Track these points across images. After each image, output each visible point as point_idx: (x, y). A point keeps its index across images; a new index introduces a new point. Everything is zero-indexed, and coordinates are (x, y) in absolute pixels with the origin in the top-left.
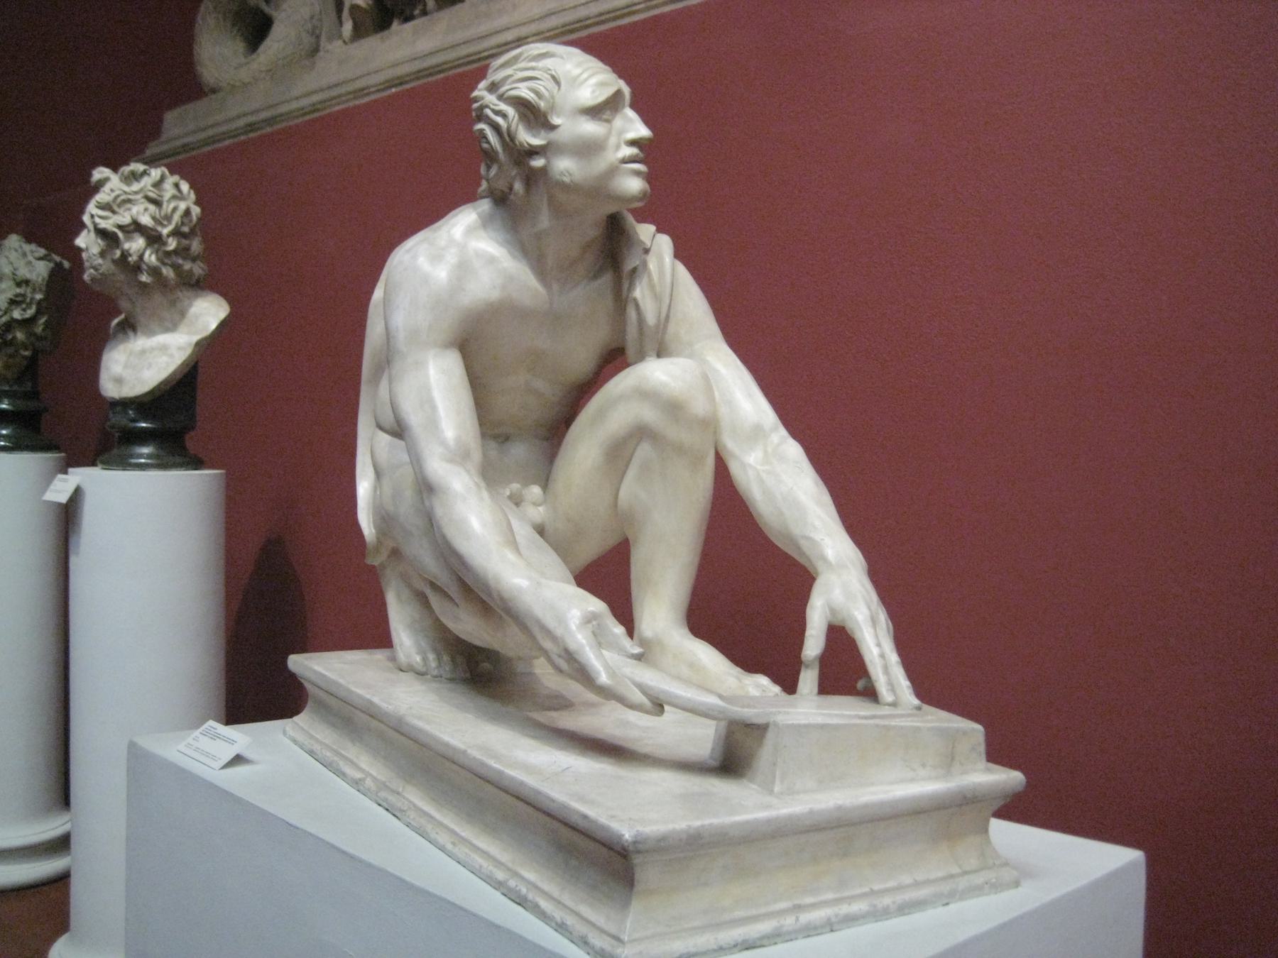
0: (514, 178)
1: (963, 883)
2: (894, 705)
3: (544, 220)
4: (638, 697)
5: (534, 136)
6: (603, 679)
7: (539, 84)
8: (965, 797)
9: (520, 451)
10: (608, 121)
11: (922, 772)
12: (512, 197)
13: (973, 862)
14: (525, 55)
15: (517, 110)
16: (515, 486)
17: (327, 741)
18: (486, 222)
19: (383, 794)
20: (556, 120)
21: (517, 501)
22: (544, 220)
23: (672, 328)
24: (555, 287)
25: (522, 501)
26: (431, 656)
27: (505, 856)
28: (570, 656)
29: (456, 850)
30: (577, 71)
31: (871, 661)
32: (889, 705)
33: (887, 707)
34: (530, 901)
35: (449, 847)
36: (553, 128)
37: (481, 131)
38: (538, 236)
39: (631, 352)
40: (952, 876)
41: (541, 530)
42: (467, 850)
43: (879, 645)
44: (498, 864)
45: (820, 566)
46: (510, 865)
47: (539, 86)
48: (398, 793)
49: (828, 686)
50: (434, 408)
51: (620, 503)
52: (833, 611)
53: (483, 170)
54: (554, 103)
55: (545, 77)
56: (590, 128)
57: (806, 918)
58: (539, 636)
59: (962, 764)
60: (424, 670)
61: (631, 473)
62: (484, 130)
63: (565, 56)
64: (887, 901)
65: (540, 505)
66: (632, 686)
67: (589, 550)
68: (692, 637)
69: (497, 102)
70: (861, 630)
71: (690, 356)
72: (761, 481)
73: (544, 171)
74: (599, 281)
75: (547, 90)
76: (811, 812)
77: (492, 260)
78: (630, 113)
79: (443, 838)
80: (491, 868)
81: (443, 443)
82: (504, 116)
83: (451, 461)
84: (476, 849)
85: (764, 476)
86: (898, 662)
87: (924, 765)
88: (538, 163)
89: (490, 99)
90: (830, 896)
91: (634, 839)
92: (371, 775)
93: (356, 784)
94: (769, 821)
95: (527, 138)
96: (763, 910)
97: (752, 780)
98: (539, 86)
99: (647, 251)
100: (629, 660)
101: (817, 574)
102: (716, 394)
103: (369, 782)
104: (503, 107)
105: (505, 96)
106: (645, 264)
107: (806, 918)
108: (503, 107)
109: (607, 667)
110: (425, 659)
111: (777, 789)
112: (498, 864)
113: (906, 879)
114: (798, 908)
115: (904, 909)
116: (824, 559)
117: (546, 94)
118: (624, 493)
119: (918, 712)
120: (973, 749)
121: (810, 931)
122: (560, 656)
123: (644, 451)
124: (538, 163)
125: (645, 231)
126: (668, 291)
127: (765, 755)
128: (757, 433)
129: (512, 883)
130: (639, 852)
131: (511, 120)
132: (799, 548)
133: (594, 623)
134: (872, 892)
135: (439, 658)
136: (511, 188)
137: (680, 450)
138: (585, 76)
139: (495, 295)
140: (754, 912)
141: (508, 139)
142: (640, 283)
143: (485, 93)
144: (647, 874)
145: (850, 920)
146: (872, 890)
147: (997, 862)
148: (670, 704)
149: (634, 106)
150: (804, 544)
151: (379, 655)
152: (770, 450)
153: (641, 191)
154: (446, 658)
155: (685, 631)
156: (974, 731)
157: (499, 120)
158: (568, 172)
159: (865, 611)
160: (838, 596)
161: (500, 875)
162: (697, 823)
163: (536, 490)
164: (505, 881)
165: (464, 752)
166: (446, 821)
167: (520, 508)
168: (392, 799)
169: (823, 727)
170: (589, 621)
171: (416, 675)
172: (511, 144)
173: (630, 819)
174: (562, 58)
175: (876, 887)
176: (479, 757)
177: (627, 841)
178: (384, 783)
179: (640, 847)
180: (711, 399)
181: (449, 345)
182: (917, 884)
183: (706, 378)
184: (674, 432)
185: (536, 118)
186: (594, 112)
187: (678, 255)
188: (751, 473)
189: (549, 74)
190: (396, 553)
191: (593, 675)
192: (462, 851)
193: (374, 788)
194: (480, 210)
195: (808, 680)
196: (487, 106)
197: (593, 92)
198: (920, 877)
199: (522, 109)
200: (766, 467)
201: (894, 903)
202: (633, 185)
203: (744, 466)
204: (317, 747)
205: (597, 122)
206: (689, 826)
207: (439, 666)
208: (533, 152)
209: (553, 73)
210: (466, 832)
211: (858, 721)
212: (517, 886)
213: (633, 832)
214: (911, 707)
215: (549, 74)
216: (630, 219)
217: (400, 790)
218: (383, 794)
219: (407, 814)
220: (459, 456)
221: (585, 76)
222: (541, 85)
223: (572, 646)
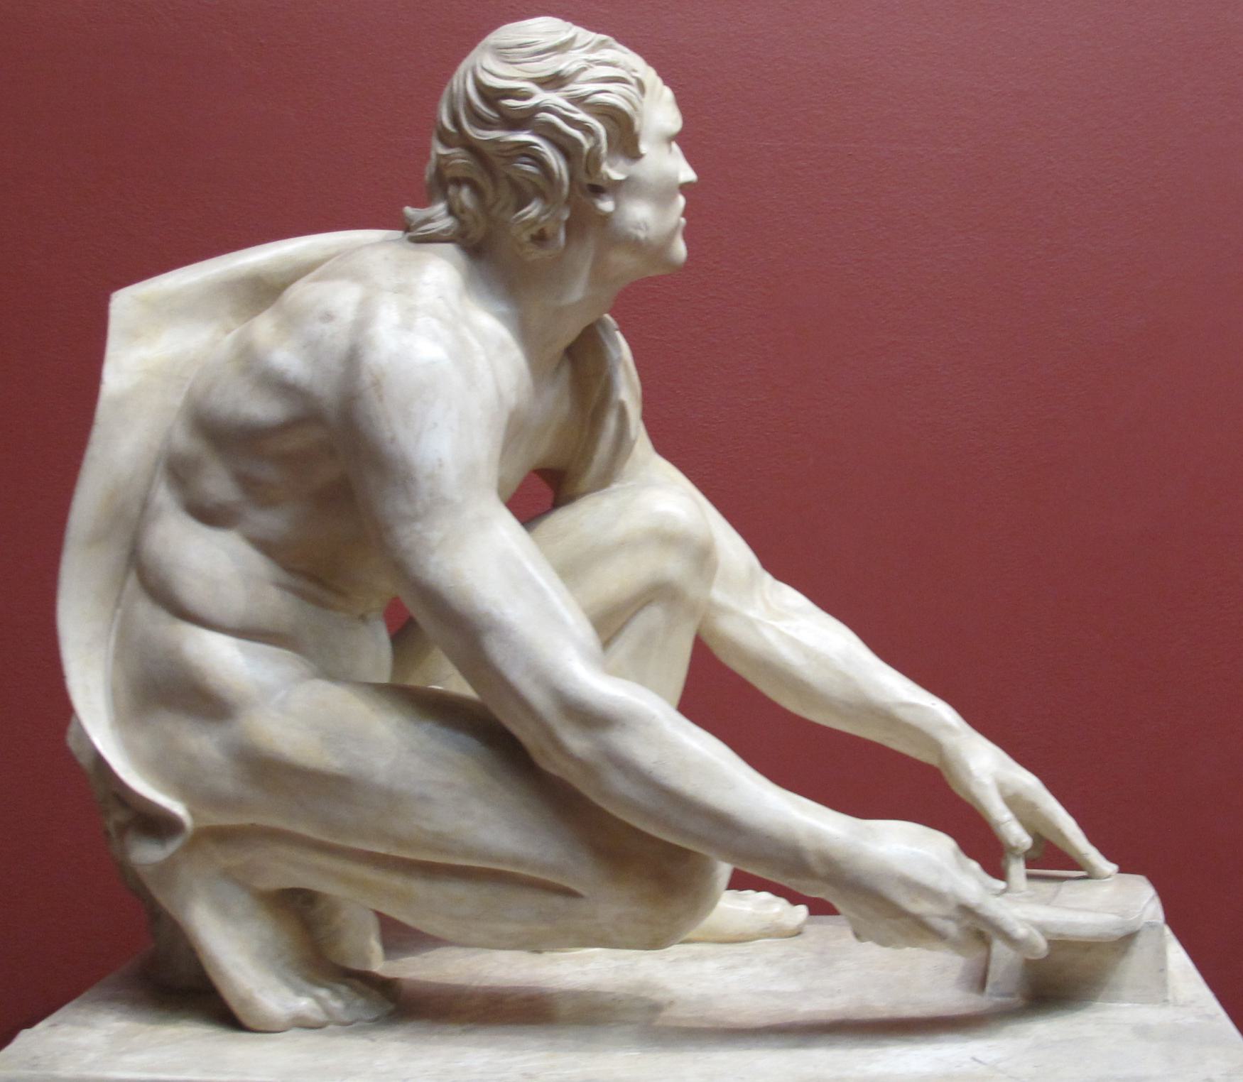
26: (323, 993)
72: (795, 643)
82: (588, 130)
88: (607, 205)
110: (318, 999)
124: (607, 205)
135: (337, 994)
158: (645, 224)
195: (1017, 870)
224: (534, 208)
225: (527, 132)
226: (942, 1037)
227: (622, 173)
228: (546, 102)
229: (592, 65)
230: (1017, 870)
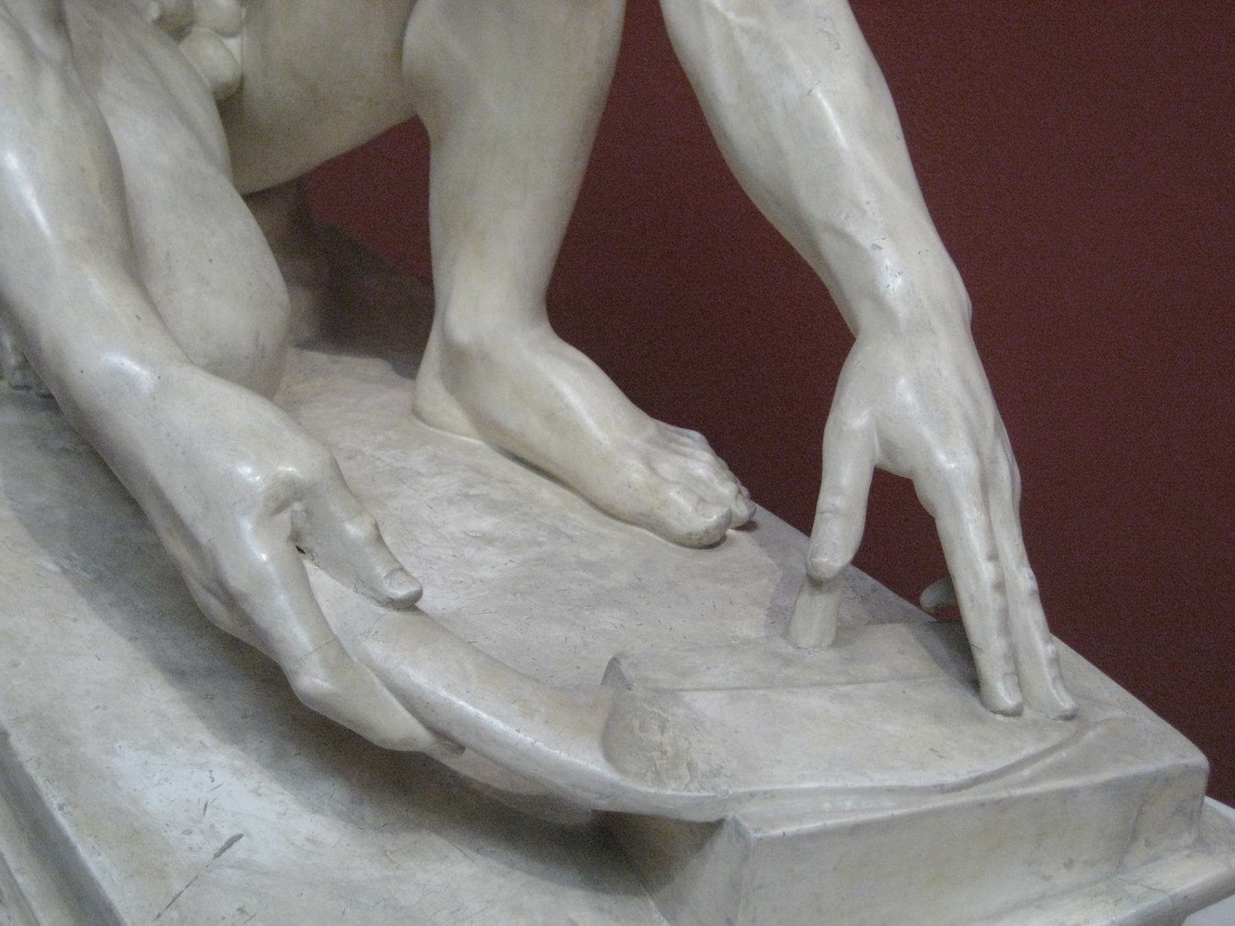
2: (1016, 713)
32: (1005, 713)
33: (999, 717)
43: (994, 557)
45: (864, 318)
51: (407, 58)
52: (888, 446)
59: (1148, 844)
65: (232, 35)
66: (386, 693)
70: (956, 511)
72: (737, 59)
85: (743, 42)
86: (1033, 592)
87: (1069, 865)
116: (879, 302)
118: (412, 39)
119: (1072, 726)
132: (813, 245)
133: (297, 506)
150: (830, 246)
155: (544, 330)
167: (183, 47)
169: (855, 830)
170: (281, 508)
176: (31, 770)
188: (713, 31)
200: (750, 21)
211: (939, 802)
223: (237, 580)
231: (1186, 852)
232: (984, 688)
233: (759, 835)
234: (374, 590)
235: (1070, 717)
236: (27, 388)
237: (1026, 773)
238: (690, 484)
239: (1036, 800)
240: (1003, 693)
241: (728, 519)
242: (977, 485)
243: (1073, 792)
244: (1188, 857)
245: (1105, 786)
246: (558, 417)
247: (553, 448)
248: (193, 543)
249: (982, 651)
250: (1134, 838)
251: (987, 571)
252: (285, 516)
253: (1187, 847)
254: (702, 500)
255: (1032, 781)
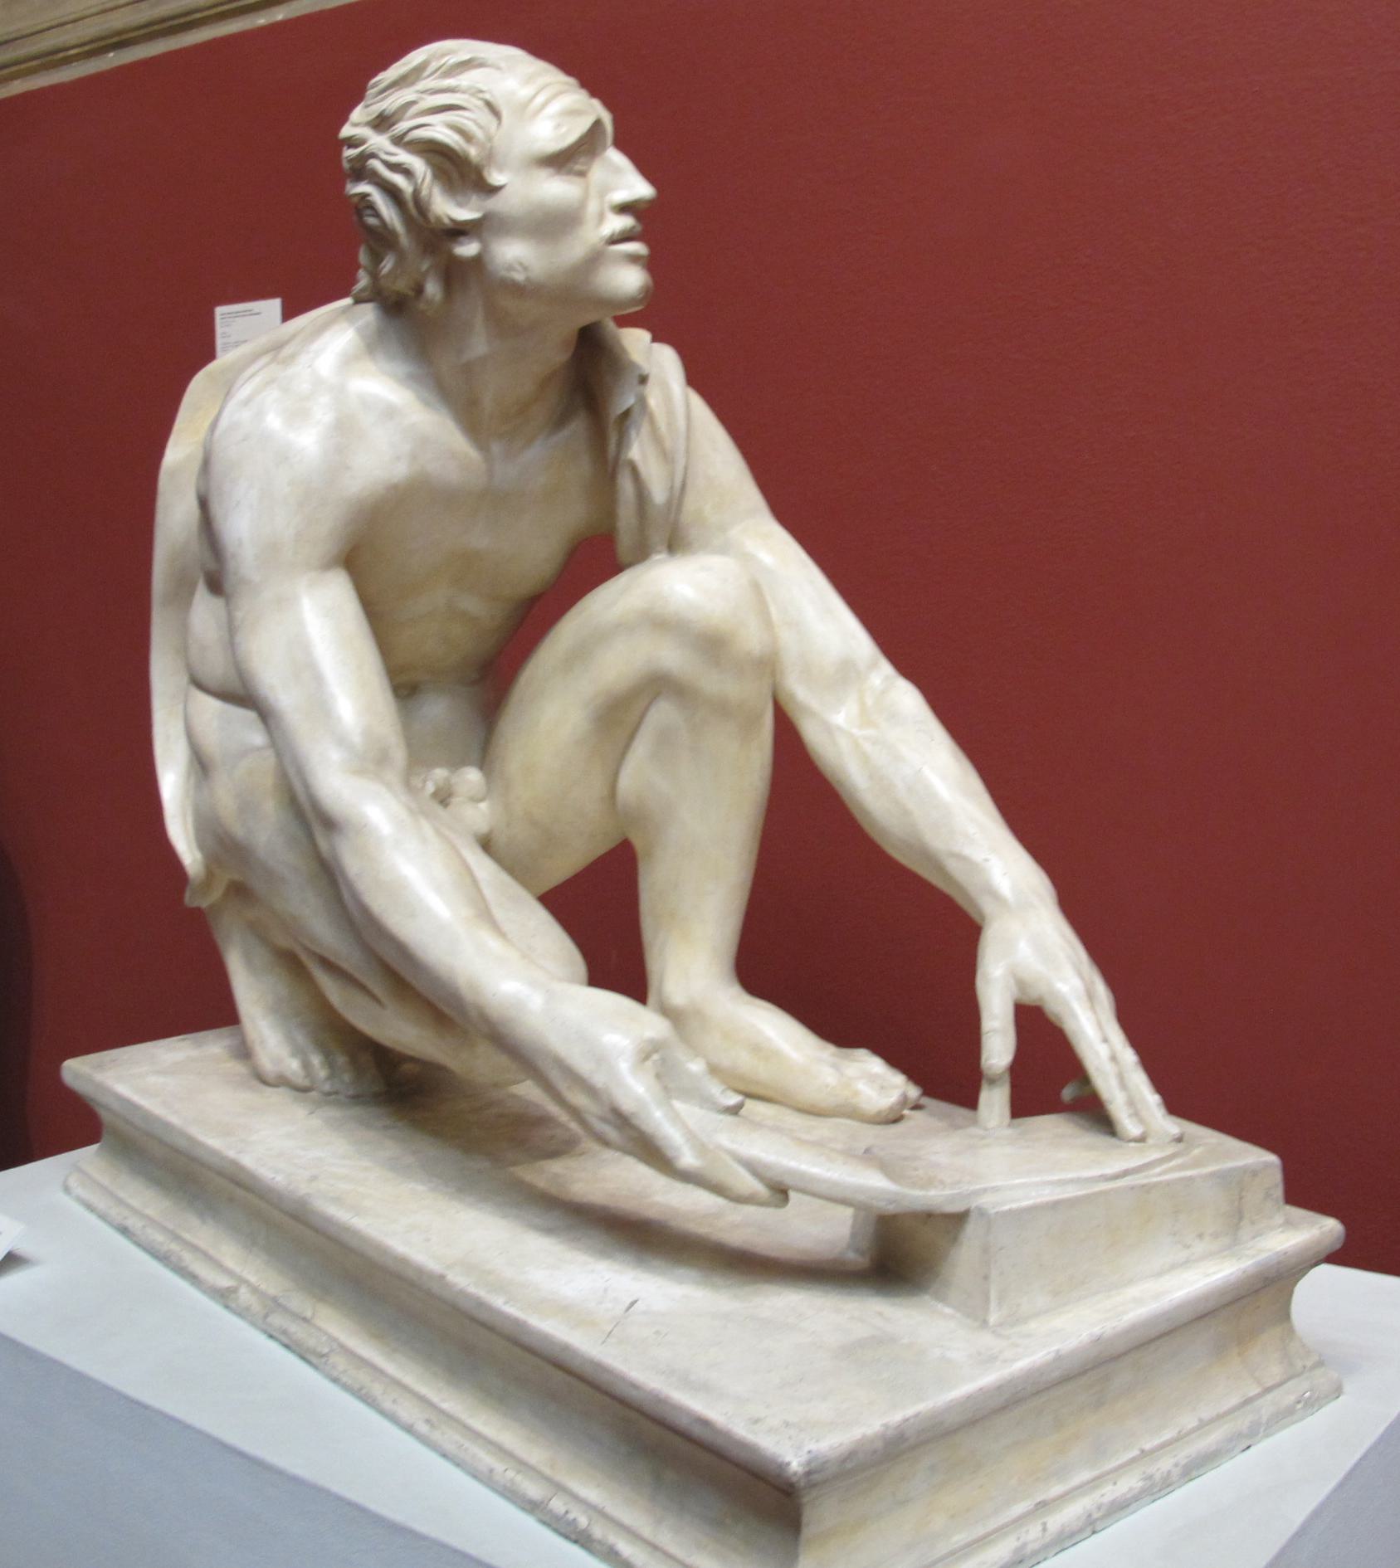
0: (425, 275)
1: (1266, 1407)
2: (1142, 1139)
3: (479, 345)
4: (748, 1183)
5: (460, 205)
6: (688, 1159)
7: (468, 119)
8: (1267, 1278)
9: (438, 709)
10: (582, 174)
11: (1200, 1247)
12: (422, 306)
13: (1274, 1371)
14: (434, 66)
15: (429, 162)
16: (440, 773)
17: (149, 1212)
18: (373, 345)
19: (277, 1320)
20: (496, 178)
21: (443, 797)
22: (479, 345)
23: (690, 504)
24: (496, 448)
25: (450, 795)
26: (316, 1060)
27: (536, 1454)
28: (621, 1120)
29: (436, 1436)
30: (525, 92)
31: (1097, 1069)
33: (1132, 1144)
34: (600, 1542)
35: (423, 1428)
36: (494, 190)
37: (364, 196)
38: (468, 369)
39: (625, 540)
40: (1248, 1401)
41: (486, 844)
42: (457, 1437)
44: (523, 1465)
45: (987, 906)
46: (548, 1471)
47: (466, 121)
48: (305, 1320)
49: (1024, 1105)
50: (318, 679)
52: (1021, 984)
53: (363, 257)
54: (491, 148)
55: (476, 106)
56: (555, 189)
57: (1057, 1520)
58: (562, 1086)
60: (306, 1083)
61: (641, 749)
62: (368, 195)
63: (503, 65)
64: (1165, 1464)
65: (481, 800)
67: (563, 867)
68: (747, 998)
69: (393, 149)
70: (1074, 1016)
71: (724, 550)
72: (865, 759)
73: (478, 262)
74: (565, 433)
75: (481, 127)
76: (1059, 1358)
77: (390, 413)
78: (615, 157)
79: (408, 1411)
80: (510, 1474)
81: (342, 741)
82: (407, 172)
83: (360, 772)
84: (476, 1436)
85: (867, 747)
87: (1201, 1236)
88: (468, 249)
89: (378, 142)
90: (1085, 1475)
91: (807, 1469)
92: (247, 1282)
93: (223, 1296)
94: (999, 1388)
95: (449, 208)
96: (992, 1524)
97: (942, 1298)
98: (466, 121)
99: (643, 380)
100: (721, 1117)
101: (983, 918)
102: (773, 610)
103: (244, 1295)
104: (403, 157)
105: (407, 139)
106: (642, 401)
107: (1057, 1520)
108: (403, 157)
109: (691, 1136)
110: (306, 1065)
111: (993, 1319)
112: (523, 1465)
113: (1189, 1421)
114: (1043, 1506)
115: (1191, 1470)
117: (479, 134)
118: (628, 781)
119: (1181, 1146)
120: (1268, 1196)
121: (1065, 1539)
122: (603, 1119)
123: (662, 713)
124: (468, 249)
125: (637, 343)
126: (681, 445)
127: (965, 1257)
128: (846, 674)
129: (558, 1505)
130: (814, 1485)
131: (420, 181)
134: (1144, 1454)
135: (330, 1063)
136: (419, 290)
137: (722, 709)
138: (540, 99)
139: (400, 471)
140: (980, 1531)
141: (414, 210)
142: (638, 434)
143: (365, 132)
144: (819, 1515)
145: (1119, 1508)
146: (1143, 1451)
147: (1309, 1364)
148: (802, 1191)
149: (621, 144)
150: (953, 866)
151: (208, 1048)
152: (869, 702)
153: (642, 287)
154: (341, 1060)
155: (736, 990)
156: (1262, 1160)
157: (399, 180)
158: (521, 264)
159: (1077, 983)
160: (1024, 951)
161: (534, 1490)
162: (896, 1417)
163: (472, 776)
164: (542, 1502)
165: (442, 1277)
166: (409, 1379)
168: (295, 1329)
169: (1055, 1205)
170: (647, 1057)
171: (297, 1093)
172: (421, 220)
173: (787, 1424)
174: (498, 68)
175: (1148, 1446)
176: (472, 1290)
177: (795, 1474)
178: (275, 1299)
179: (816, 1477)
180: (767, 622)
181: (328, 565)
182: (1203, 1425)
183: (756, 587)
184: (713, 683)
185: (463, 176)
186: (561, 161)
187: (695, 379)
188: (844, 743)
189: (482, 99)
190: (240, 891)
191: (670, 1153)
192: (449, 1438)
193: (256, 1306)
194: (361, 323)
195: (995, 1100)
196: (373, 156)
197: (558, 126)
198: (1206, 1413)
199: (438, 159)
201: (1176, 1465)
202: (628, 280)
203: (828, 728)
204: (133, 1223)
205: (564, 177)
206: (886, 1426)
207: (331, 1077)
208: (459, 231)
209: (487, 96)
210: (452, 1401)
212: (567, 1512)
213: (804, 1458)
214: (1167, 1140)
215: (482, 99)
216: (611, 325)
217: (308, 1314)
218: (277, 1320)
219: (331, 1361)
220: (371, 762)
221: (540, 99)
222: (468, 119)
223: (627, 1105)
224: (388, 262)
225: (366, 181)
226: (682, 1271)
227: (478, 211)
228: (370, 148)
229: (423, 96)
230: (995, 1100)
231: (1280, 1230)
232: (1119, 1128)
233: (995, 1210)
234: (714, 1103)
235: (1179, 1140)
236: (336, 1093)
237: (1158, 1170)
238: (872, 1078)
239: (1168, 1185)
240: (1129, 1125)
241: (904, 1102)
242: (1085, 998)
243: (1191, 1179)
244: (1282, 1232)
245: (1213, 1175)
246: (759, 1049)
247: (762, 1072)
248: (591, 1091)
249: (1111, 1104)
250: (1241, 1218)
251: (1103, 1051)
252: (649, 1063)
253: (1280, 1226)
254: (882, 1088)
255: (1160, 1174)
